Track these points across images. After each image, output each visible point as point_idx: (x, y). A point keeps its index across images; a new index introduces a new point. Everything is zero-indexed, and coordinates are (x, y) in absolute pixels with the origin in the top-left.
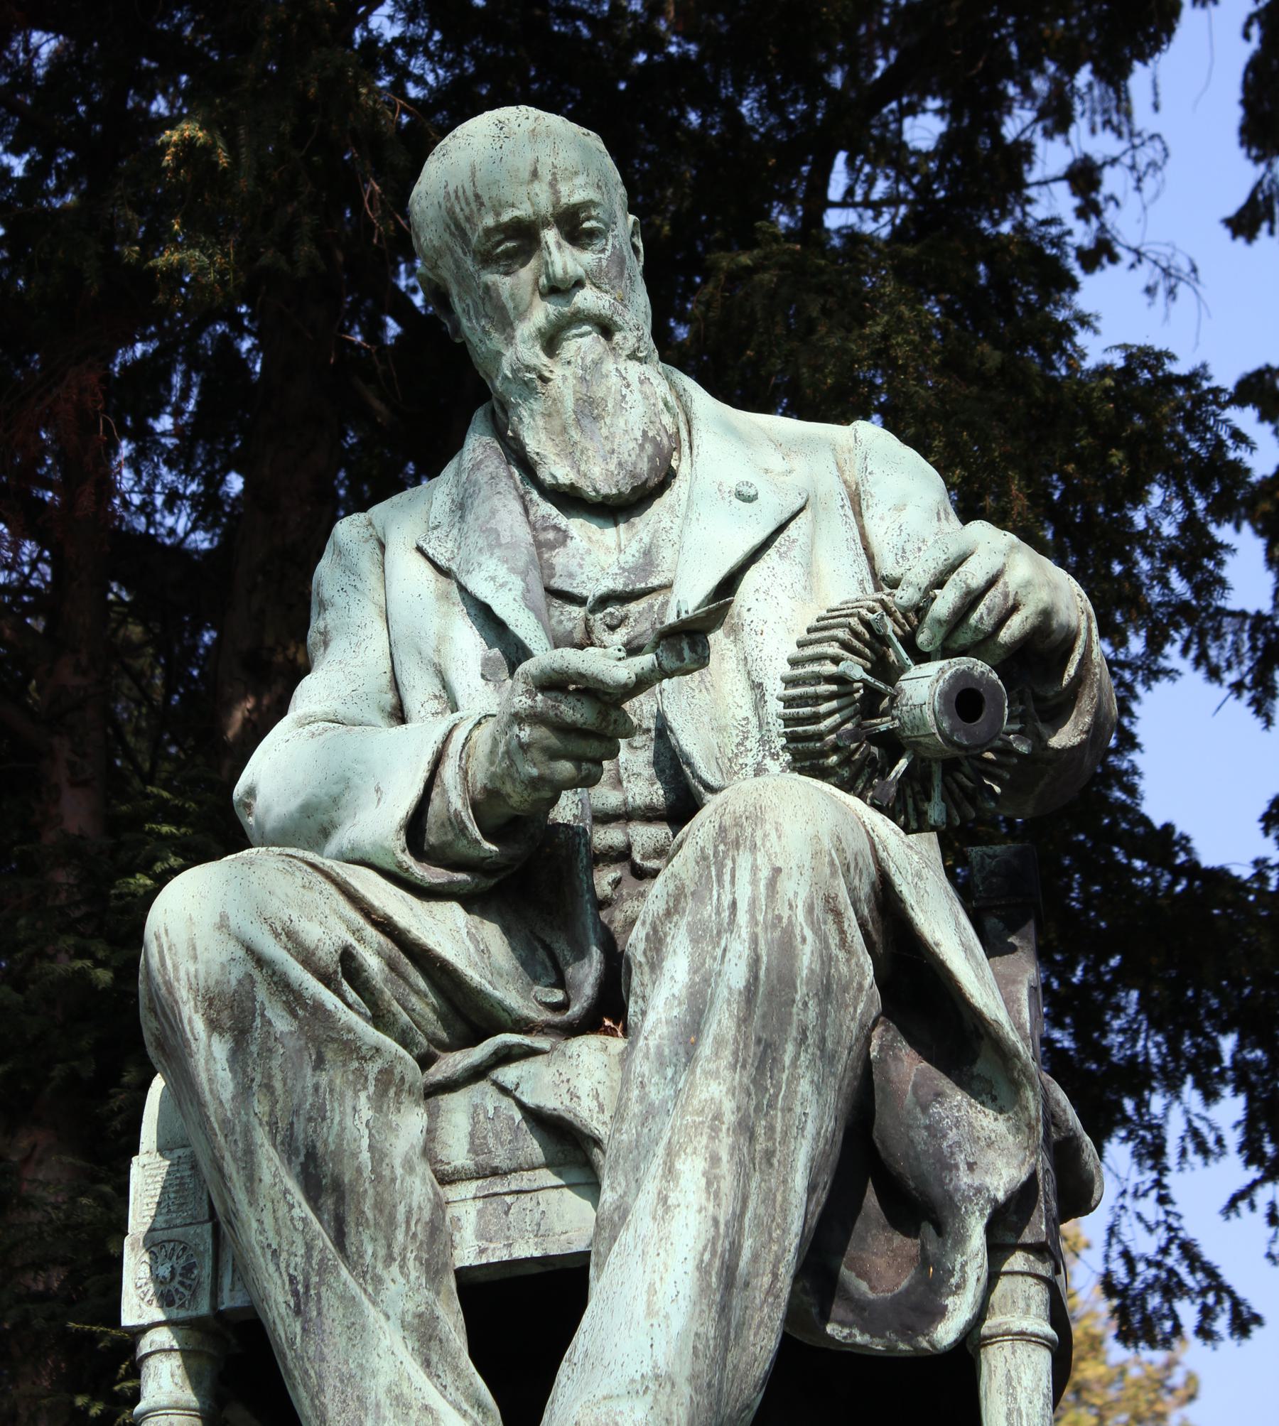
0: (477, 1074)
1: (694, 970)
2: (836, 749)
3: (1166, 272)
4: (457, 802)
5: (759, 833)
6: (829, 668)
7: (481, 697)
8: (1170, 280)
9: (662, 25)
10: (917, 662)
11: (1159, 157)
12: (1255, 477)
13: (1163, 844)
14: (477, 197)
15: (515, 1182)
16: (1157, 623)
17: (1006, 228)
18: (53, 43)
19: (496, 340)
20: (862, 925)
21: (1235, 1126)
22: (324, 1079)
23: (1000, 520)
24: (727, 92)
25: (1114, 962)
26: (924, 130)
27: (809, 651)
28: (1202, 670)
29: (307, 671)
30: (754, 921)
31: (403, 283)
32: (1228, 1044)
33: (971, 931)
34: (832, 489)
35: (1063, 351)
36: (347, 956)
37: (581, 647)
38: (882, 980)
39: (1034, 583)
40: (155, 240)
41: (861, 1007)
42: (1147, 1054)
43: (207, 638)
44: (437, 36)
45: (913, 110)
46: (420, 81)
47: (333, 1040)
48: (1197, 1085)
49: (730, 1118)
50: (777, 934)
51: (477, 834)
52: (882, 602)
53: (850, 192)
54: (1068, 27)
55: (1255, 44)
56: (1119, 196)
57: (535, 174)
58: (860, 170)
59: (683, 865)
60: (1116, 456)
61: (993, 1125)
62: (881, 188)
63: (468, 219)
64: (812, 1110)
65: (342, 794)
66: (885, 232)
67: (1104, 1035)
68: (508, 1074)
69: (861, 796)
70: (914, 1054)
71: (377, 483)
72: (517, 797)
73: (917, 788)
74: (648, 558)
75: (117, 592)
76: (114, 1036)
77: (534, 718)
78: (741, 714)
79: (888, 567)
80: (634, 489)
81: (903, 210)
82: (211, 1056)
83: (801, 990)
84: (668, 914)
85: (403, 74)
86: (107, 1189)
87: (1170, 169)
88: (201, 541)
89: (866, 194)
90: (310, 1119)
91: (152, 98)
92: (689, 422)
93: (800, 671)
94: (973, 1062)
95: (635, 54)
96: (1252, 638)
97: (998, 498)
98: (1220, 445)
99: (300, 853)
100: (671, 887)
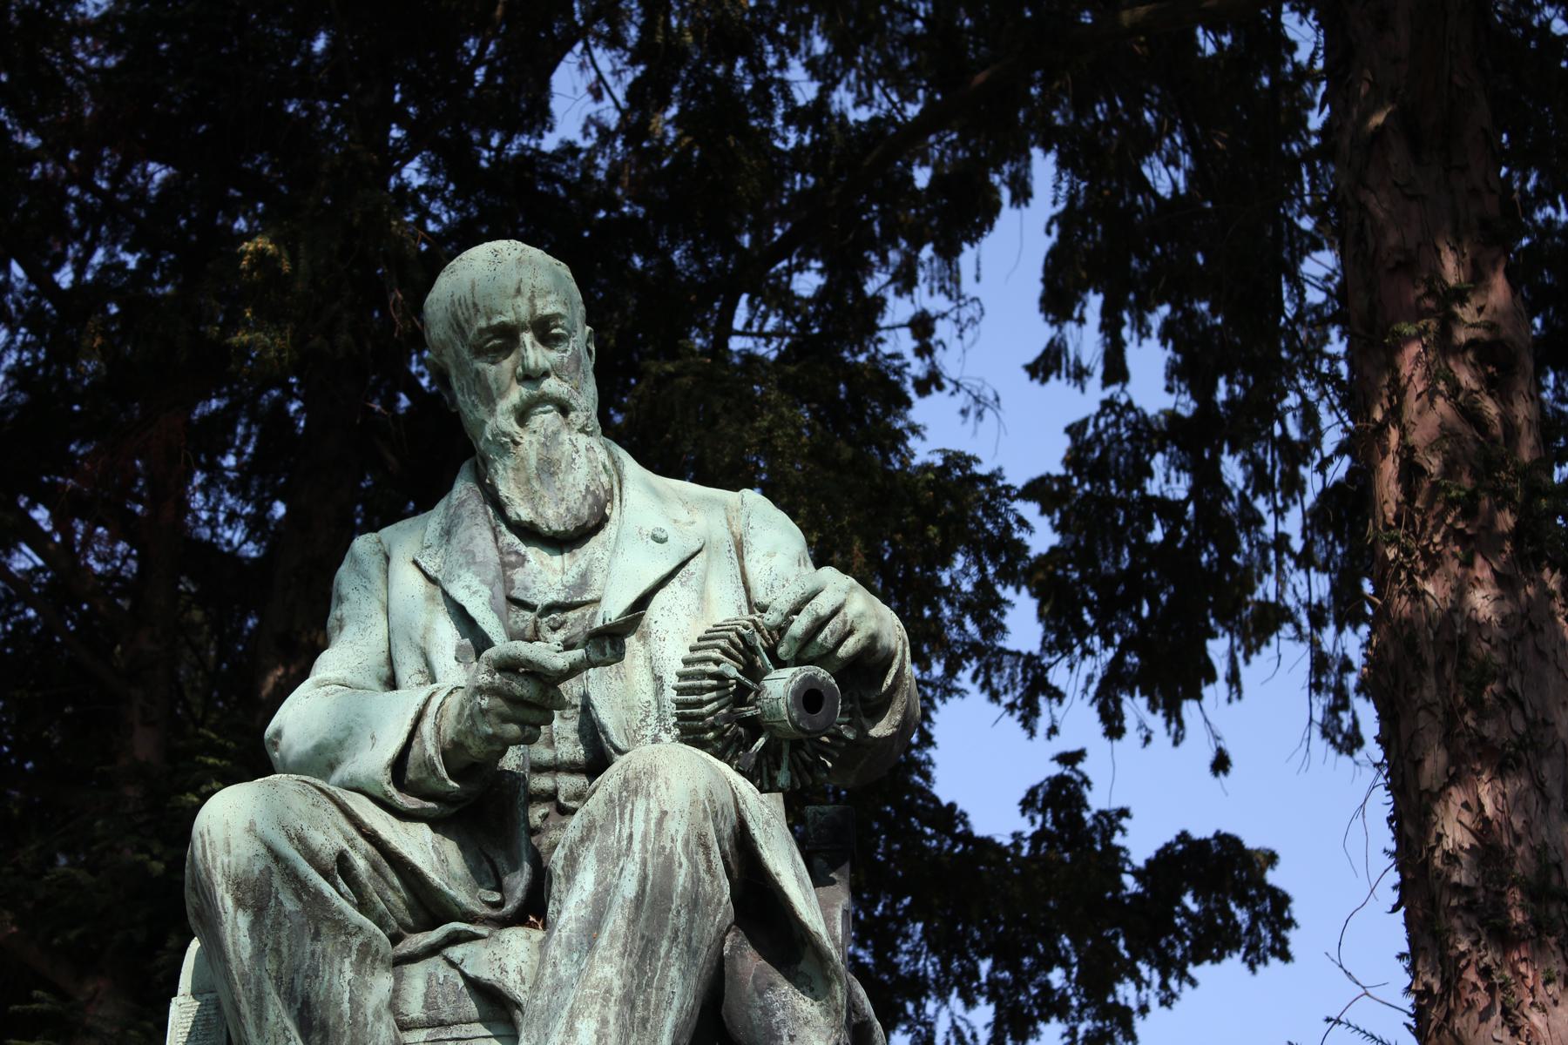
0: (433, 950)
1: (598, 883)
2: (713, 727)
3: (977, 400)
4: (431, 750)
5: (653, 785)
6: (712, 668)
7: (453, 673)
8: (979, 406)
9: (619, 192)
10: (777, 668)
11: (977, 315)
12: (1032, 554)
13: (948, 817)
14: (475, 305)
15: (456, 1032)
16: (953, 654)
17: (862, 358)
18: (164, 172)
19: (482, 411)
20: (724, 858)
21: (986, 1026)
22: (319, 947)
23: (845, 569)
24: (663, 243)
25: (907, 901)
26: (807, 283)
27: (698, 654)
28: (986, 693)
29: (325, 646)
30: (644, 849)
31: (414, 369)
32: (985, 966)
33: (803, 866)
34: (721, 534)
35: (898, 451)
36: (342, 858)
37: (531, 641)
38: (734, 897)
39: (868, 616)
40: (233, 324)
41: (719, 916)
42: (926, 970)
43: (250, 623)
44: (452, 187)
45: (800, 268)
46: (437, 219)
47: (328, 919)
48: (961, 995)
49: (617, 992)
50: (661, 860)
51: (445, 774)
52: (754, 622)
53: (749, 324)
54: (918, 215)
55: (1054, 238)
56: (946, 341)
57: (518, 291)
58: (757, 308)
59: (595, 805)
60: (933, 531)
61: (810, 1009)
62: (772, 322)
63: (467, 321)
64: (678, 990)
65: (345, 739)
66: (773, 355)
67: (895, 955)
68: (456, 952)
69: (730, 763)
70: (755, 954)
71: (384, 515)
72: (475, 748)
73: (771, 759)
74: (584, 581)
75: (186, 585)
76: (165, 905)
77: (492, 691)
78: (646, 698)
79: (760, 596)
80: (577, 528)
81: (787, 340)
82: (237, 927)
83: (676, 902)
84: (582, 840)
85: (425, 214)
86: (150, 1025)
87: (984, 324)
88: (251, 550)
89: (761, 327)
90: (307, 977)
91: (235, 219)
92: (620, 482)
93: (691, 669)
94: (798, 962)
95: (597, 211)
96: (1024, 672)
97: (843, 555)
98: (1008, 528)
99: (312, 780)
100: (586, 821)
